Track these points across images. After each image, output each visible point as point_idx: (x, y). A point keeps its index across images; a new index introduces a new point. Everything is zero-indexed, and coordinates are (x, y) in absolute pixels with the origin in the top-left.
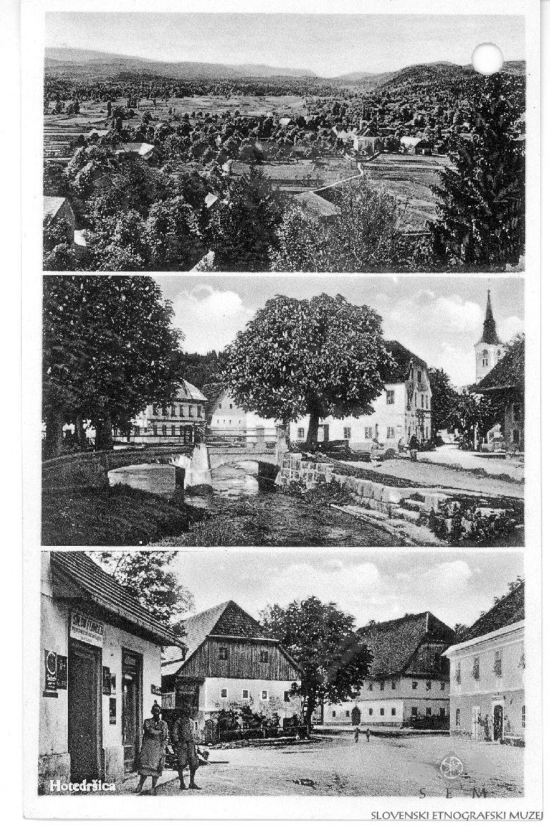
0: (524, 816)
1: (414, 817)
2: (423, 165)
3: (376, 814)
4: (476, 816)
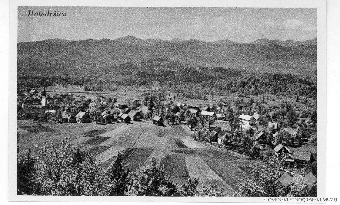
0: (329, 200)
1: (282, 200)
2: (262, 141)
3: (265, 199)
4: (308, 200)
